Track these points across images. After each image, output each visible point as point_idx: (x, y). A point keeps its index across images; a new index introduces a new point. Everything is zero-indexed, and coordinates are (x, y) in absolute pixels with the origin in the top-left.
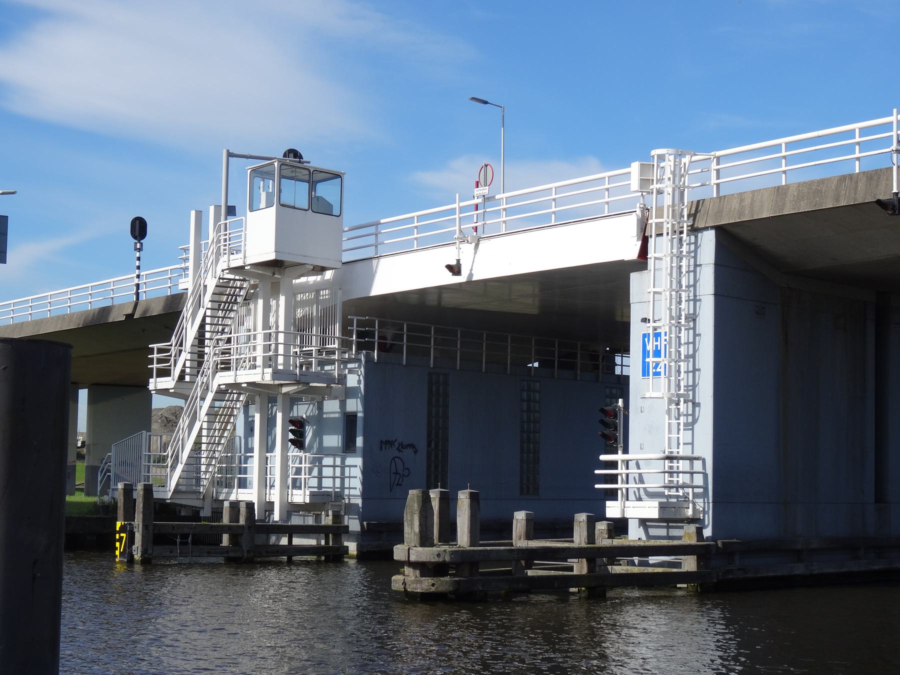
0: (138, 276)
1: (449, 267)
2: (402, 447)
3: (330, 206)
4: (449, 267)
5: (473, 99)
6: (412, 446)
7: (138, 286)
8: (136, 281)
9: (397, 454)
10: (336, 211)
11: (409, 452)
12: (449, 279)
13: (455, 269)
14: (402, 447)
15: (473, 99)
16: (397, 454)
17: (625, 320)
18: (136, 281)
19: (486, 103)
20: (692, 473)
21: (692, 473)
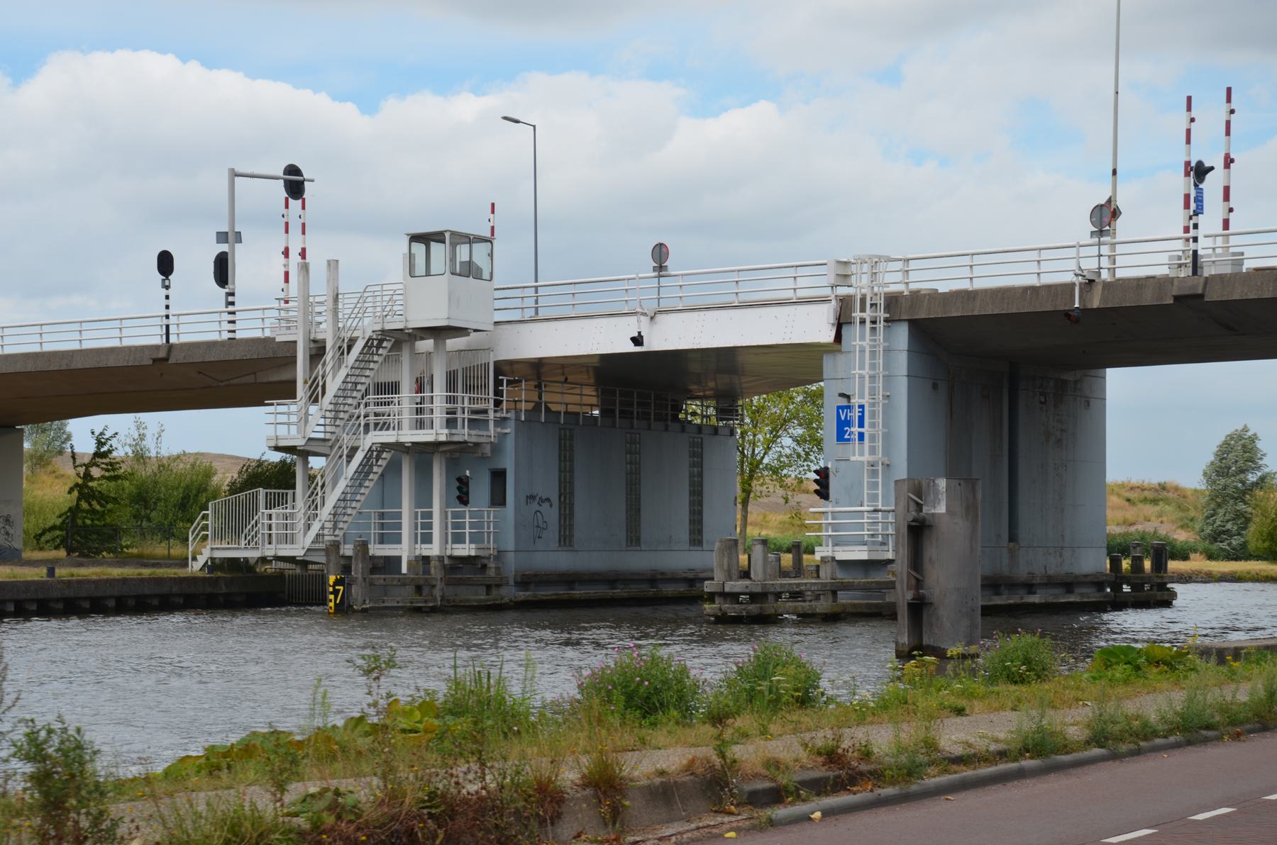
0: (167, 317)
1: (633, 339)
2: (542, 501)
3: (480, 270)
4: (633, 339)
5: (505, 118)
6: (548, 500)
7: (168, 327)
8: (165, 321)
9: (538, 508)
10: (486, 275)
11: (546, 505)
12: (631, 348)
13: (637, 341)
14: (542, 501)
15: (505, 118)
16: (538, 508)
17: (595, 360)
18: (165, 321)
19: (517, 122)
20: (1100, 256)
21: (1100, 256)
